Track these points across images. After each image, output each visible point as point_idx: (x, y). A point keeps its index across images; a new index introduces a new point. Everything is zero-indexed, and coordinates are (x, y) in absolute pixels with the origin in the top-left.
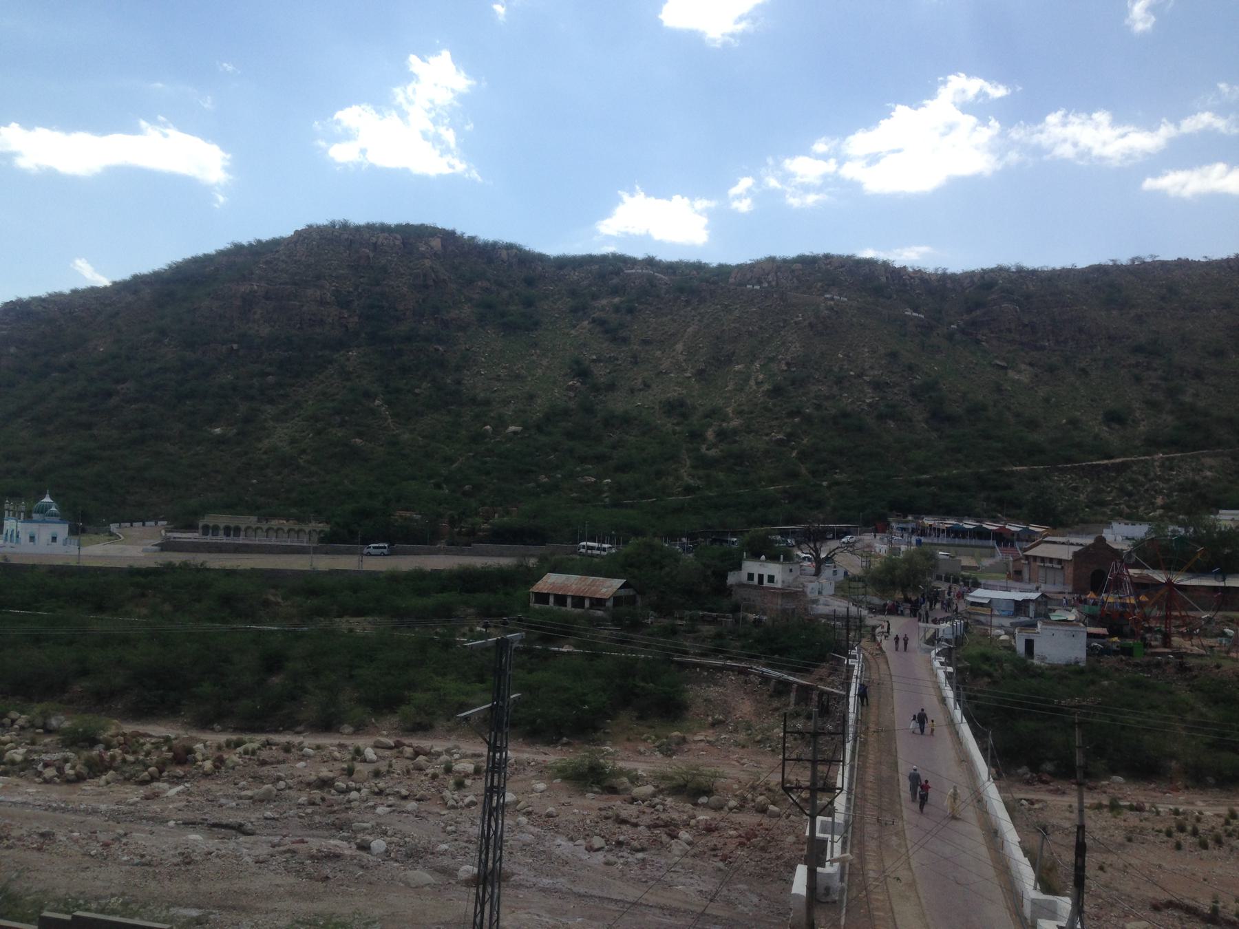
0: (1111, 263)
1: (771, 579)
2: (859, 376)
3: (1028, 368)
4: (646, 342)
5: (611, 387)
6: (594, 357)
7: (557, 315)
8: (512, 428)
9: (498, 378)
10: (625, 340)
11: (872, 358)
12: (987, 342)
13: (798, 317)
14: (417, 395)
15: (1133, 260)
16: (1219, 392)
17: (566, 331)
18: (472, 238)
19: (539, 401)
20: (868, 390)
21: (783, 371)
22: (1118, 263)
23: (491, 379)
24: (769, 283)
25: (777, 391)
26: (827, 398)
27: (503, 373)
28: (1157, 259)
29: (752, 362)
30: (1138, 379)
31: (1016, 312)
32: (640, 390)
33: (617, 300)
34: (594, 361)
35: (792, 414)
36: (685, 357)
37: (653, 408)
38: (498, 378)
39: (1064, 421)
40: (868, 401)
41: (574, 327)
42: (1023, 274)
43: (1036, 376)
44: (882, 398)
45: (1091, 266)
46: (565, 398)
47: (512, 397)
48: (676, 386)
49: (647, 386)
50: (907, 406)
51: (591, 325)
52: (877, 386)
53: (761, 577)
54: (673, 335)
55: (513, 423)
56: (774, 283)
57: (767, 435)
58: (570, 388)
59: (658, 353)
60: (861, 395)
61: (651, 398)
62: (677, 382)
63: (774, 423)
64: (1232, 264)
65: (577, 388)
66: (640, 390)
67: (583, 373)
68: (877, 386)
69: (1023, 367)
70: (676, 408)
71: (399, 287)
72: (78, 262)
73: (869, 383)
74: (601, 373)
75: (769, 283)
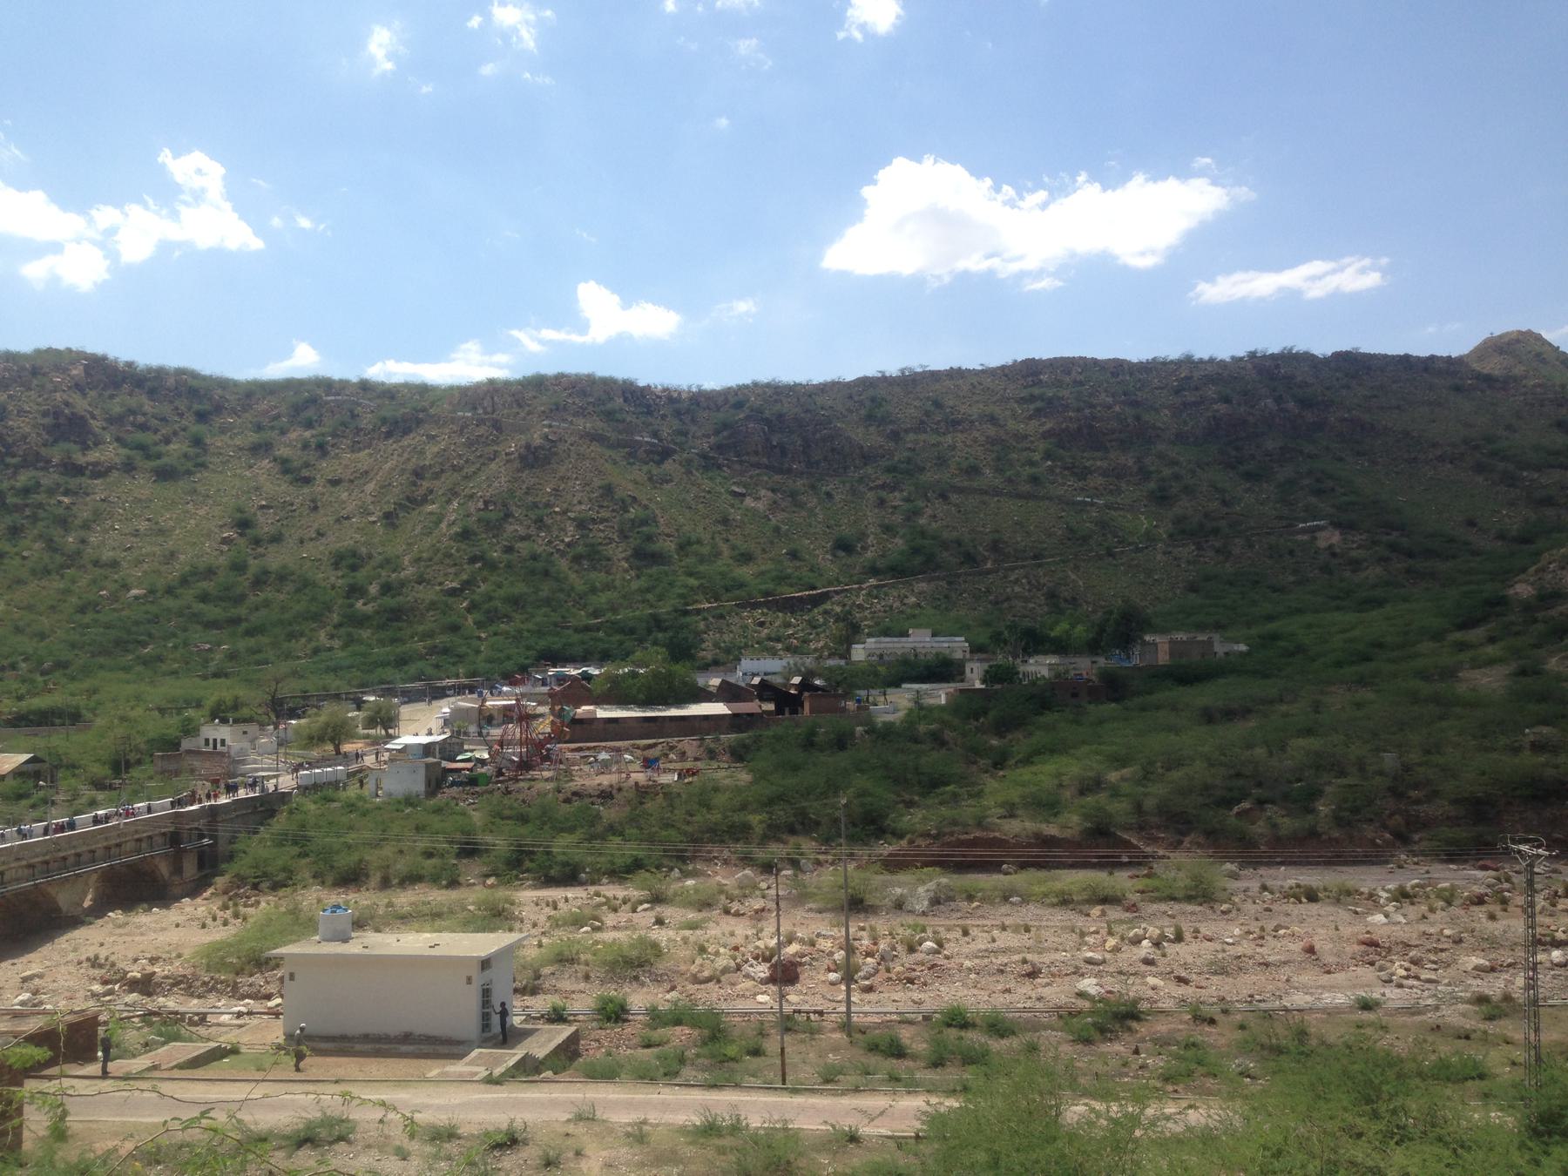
0: (880, 375)
1: (223, 742)
2: (564, 512)
3: (770, 494)
4: (335, 483)
5: (277, 539)
6: (264, 503)
7: (231, 453)
8: (135, 592)
9: (136, 533)
10: (307, 481)
11: (583, 491)
12: (729, 467)
13: (510, 447)
14: (24, 558)
15: (902, 371)
16: (960, 511)
17: (238, 471)
18: (130, 364)
19: (182, 557)
20: (571, 528)
21: (480, 510)
22: (888, 374)
23: (125, 535)
24: (484, 408)
25: (465, 535)
26: (523, 539)
27: (143, 526)
28: (928, 369)
29: (449, 502)
30: (882, 503)
31: (764, 432)
32: (311, 539)
33: (307, 434)
34: (263, 507)
35: (473, 560)
36: (373, 499)
37: (320, 560)
38: (136, 533)
39: (784, 551)
40: (567, 540)
41: (251, 467)
42: (779, 390)
43: (775, 502)
44: (582, 536)
45: (1116, 360)
46: (215, 553)
47: (147, 555)
48: (355, 532)
49: (320, 534)
50: (611, 543)
51: (271, 465)
52: (581, 524)
53: (215, 740)
54: (366, 472)
55: (137, 587)
56: (489, 409)
57: (440, 584)
58: (225, 541)
59: (344, 495)
60: (562, 533)
61: (321, 548)
62: (358, 528)
63: (450, 570)
64: (1006, 371)
65: (232, 540)
66: (311, 539)
67: (244, 525)
68: (581, 524)
69: (763, 492)
70: (348, 560)
71: (20, 428)
72: (1372, 279)
73: (574, 520)
74: (266, 524)
75: (484, 408)
